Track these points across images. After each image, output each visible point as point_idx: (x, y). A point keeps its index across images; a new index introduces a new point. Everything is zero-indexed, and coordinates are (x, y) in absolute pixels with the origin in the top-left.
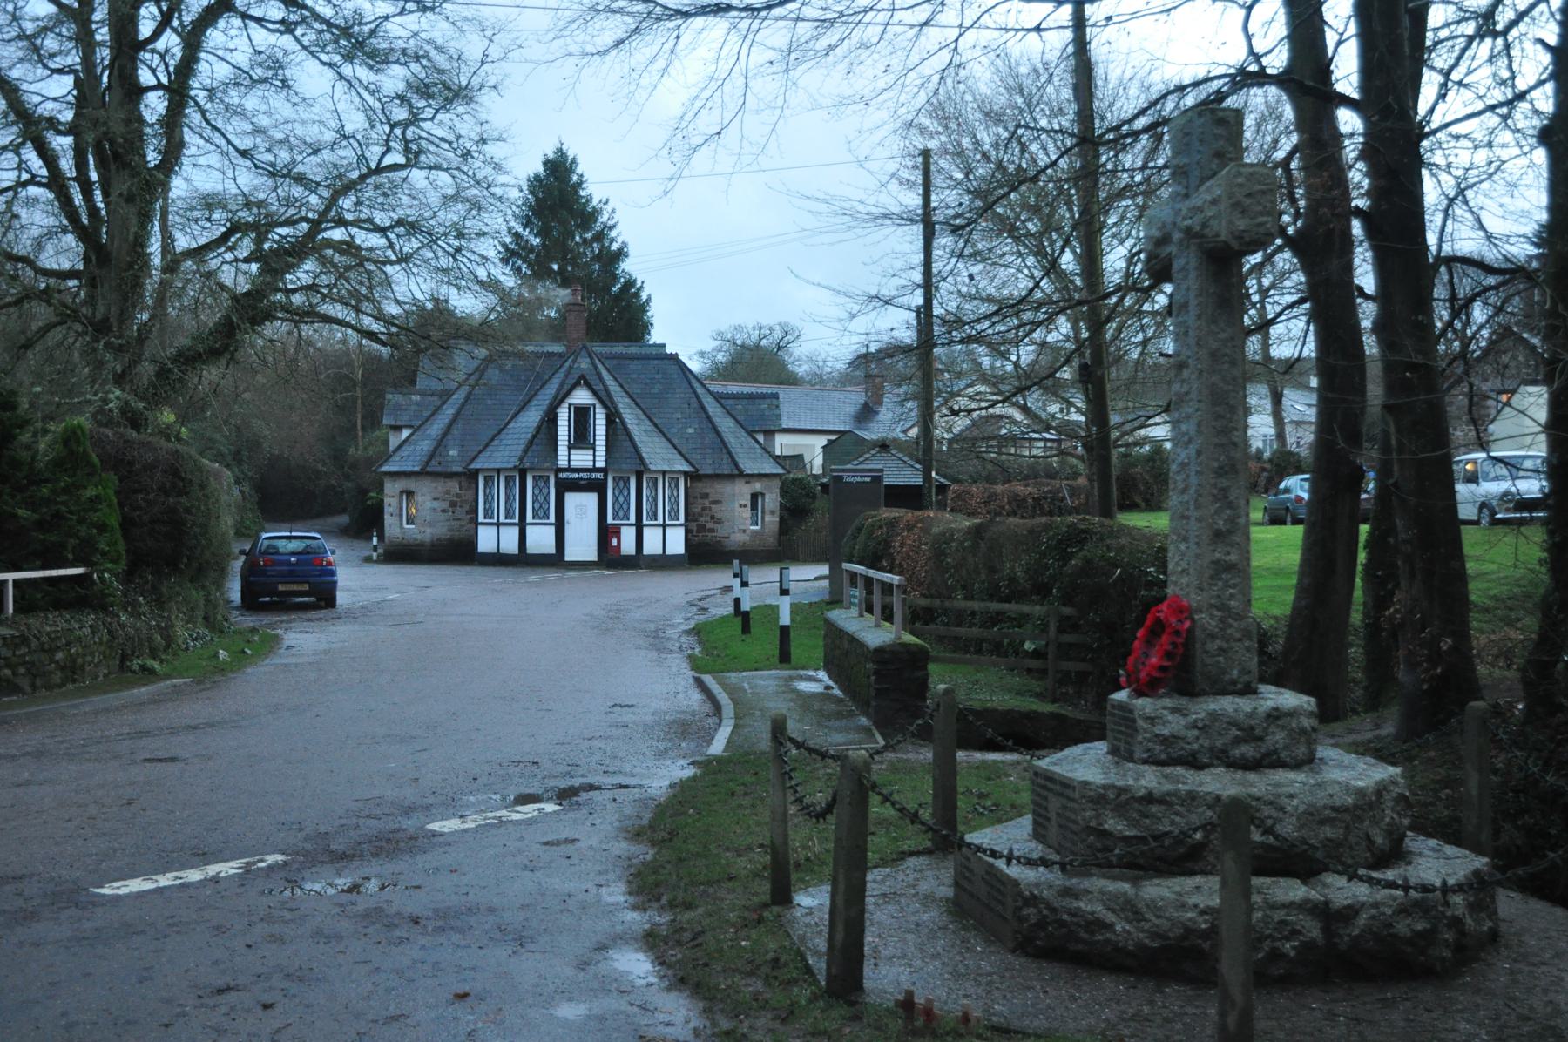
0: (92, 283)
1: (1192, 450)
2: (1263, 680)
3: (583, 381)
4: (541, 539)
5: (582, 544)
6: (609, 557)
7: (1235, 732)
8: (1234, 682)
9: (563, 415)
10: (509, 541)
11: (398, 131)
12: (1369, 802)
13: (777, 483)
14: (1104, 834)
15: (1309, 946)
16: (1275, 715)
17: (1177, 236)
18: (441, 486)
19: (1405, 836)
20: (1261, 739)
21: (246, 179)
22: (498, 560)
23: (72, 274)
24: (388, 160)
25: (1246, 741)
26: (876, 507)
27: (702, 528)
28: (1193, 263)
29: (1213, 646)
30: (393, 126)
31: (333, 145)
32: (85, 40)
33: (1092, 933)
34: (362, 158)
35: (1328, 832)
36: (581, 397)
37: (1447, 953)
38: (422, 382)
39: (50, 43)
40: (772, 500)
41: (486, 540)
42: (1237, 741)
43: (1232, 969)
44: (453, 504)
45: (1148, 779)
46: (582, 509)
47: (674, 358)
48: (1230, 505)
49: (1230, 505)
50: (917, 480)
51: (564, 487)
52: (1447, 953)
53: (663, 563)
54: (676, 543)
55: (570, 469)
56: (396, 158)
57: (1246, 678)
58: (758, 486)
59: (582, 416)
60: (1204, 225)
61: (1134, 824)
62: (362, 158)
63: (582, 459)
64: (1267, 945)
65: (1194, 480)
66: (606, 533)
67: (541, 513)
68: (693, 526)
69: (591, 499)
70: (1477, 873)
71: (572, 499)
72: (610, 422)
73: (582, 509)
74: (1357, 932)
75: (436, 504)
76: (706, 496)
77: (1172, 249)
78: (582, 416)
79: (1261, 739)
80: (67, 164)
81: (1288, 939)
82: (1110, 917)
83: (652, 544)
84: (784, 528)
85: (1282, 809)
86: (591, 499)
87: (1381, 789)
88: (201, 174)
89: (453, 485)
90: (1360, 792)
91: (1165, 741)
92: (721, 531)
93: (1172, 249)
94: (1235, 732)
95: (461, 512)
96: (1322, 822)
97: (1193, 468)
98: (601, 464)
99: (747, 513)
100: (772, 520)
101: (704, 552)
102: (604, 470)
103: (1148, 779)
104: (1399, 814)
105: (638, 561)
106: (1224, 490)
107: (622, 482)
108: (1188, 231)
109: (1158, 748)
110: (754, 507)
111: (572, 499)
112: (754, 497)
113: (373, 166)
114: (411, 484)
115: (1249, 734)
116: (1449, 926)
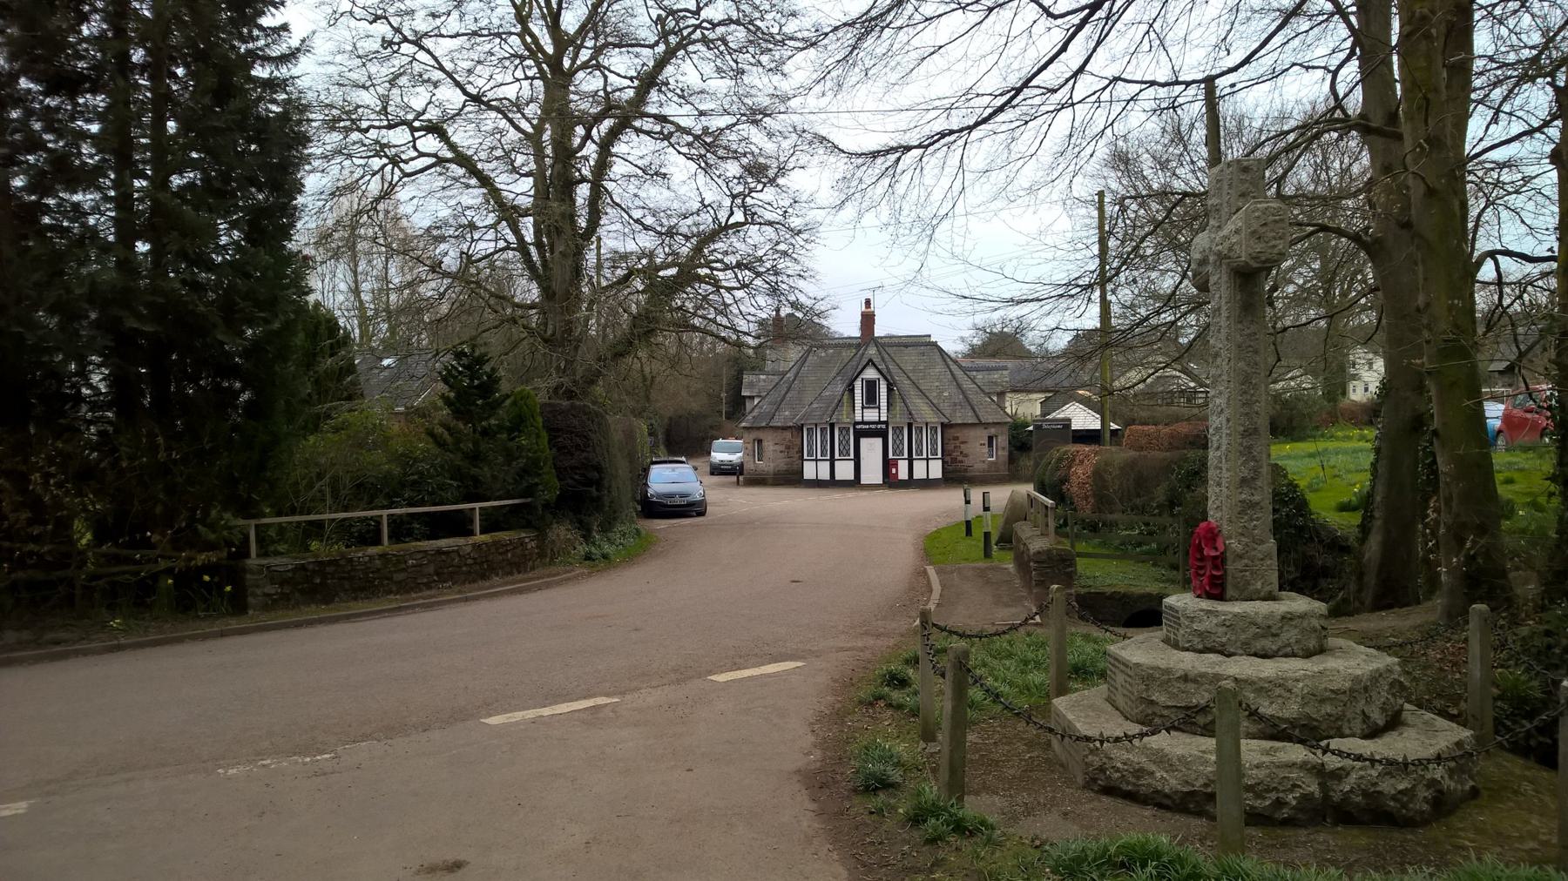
0: (543, 312)
1: (1223, 418)
2: (1281, 588)
3: (871, 362)
4: (845, 470)
5: (872, 472)
6: (890, 480)
7: (1254, 630)
8: (1258, 591)
9: (858, 384)
10: (824, 474)
11: (738, 201)
12: (1363, 688)
13: (1005, 429)
14: (1152, 702)
15: (1306, 798)
16: (1287, 618)
17: (1211, 258)
18: (779, 435)
19: (1401, 710)
20: (1276, 635)
21: (647, 241)
22: (817, 484)
23: (532, 306)
24: (732, 221)
25: (1263, 636)
26: (1067, 443)
27: (954, 460)
28: (1225, 278)
29: (1240, 565)
30: (734, 197)
31: (698, 213)
32: (539, 155)
33: (1138, 778)
34: (715, 219)
35: (1328, 708)
36: (870, 374)
37: (1425, 807)
38: (769, 366)
39: (520, 159)
40: (1003, 440)
41: (809, 471)
42: (1256, 637)
43: (1228, 809)
44: (788, 448)
45: (1187, 661)
46: (872, 450)
47: (935, 344)
48: (1254, 459)
49: (1254, 459)
50: (1097, 425)
51: (859, 435)
52: (1425, 807)
53: (927, 484)
54: (936, 470)
55: (863, 423)
56: (739, 216)
57: (1268, 588)
58: (993, 431)
59: (871, 387)
60: (1230, 249)
61: (1173, 696)
62: (715, 219)
63: (871, 415)
64: (1273, 796)
65: (1224, 441)
66: (888, 465)
67: (844, 452)
68: (948, 459)
69: (878, 442)
70: (1459, 744)
71: (865, 443)
72: (890, 390)
73: (872, 450)
74: (1348, 788)
75: (779, 448)
76: (956, 438)
77: (1210, 268)
78: (871, 387)
79: (1276, 635)
80: (529, 237)
81: (1291, 791)
82: (1153, 768)
83: (920, 473)
84: (1012, 459)
85: (1290, 691)
86: (878, 442)
87: (1376, 677)
88: (614, 238)
89: (788, 435)
90: (1356, 680)
91: (1200, 634)
92: (967, 462)
93: (1210, 268)
94: (1254, 630)
95: (793, 452)
96: (1322, 701)
97: (1225, 431)
98: (884, 418)
99: (986, 449)
100: (1004, 454)
101: (954, 476)
102: (886, 423)
103: (1187, 661)
104: (1394, 695)
105: (911, 483)
106: (1250, 447)
107: (898, 430)
108: (1219, 254)
109: (1196, 640)
110: (990, 444)
111: (864, 442)
112: (990, 439)
113: (723, 221)
114: (761, 435)
115: (1268, 631)
116: (1428, 786)
